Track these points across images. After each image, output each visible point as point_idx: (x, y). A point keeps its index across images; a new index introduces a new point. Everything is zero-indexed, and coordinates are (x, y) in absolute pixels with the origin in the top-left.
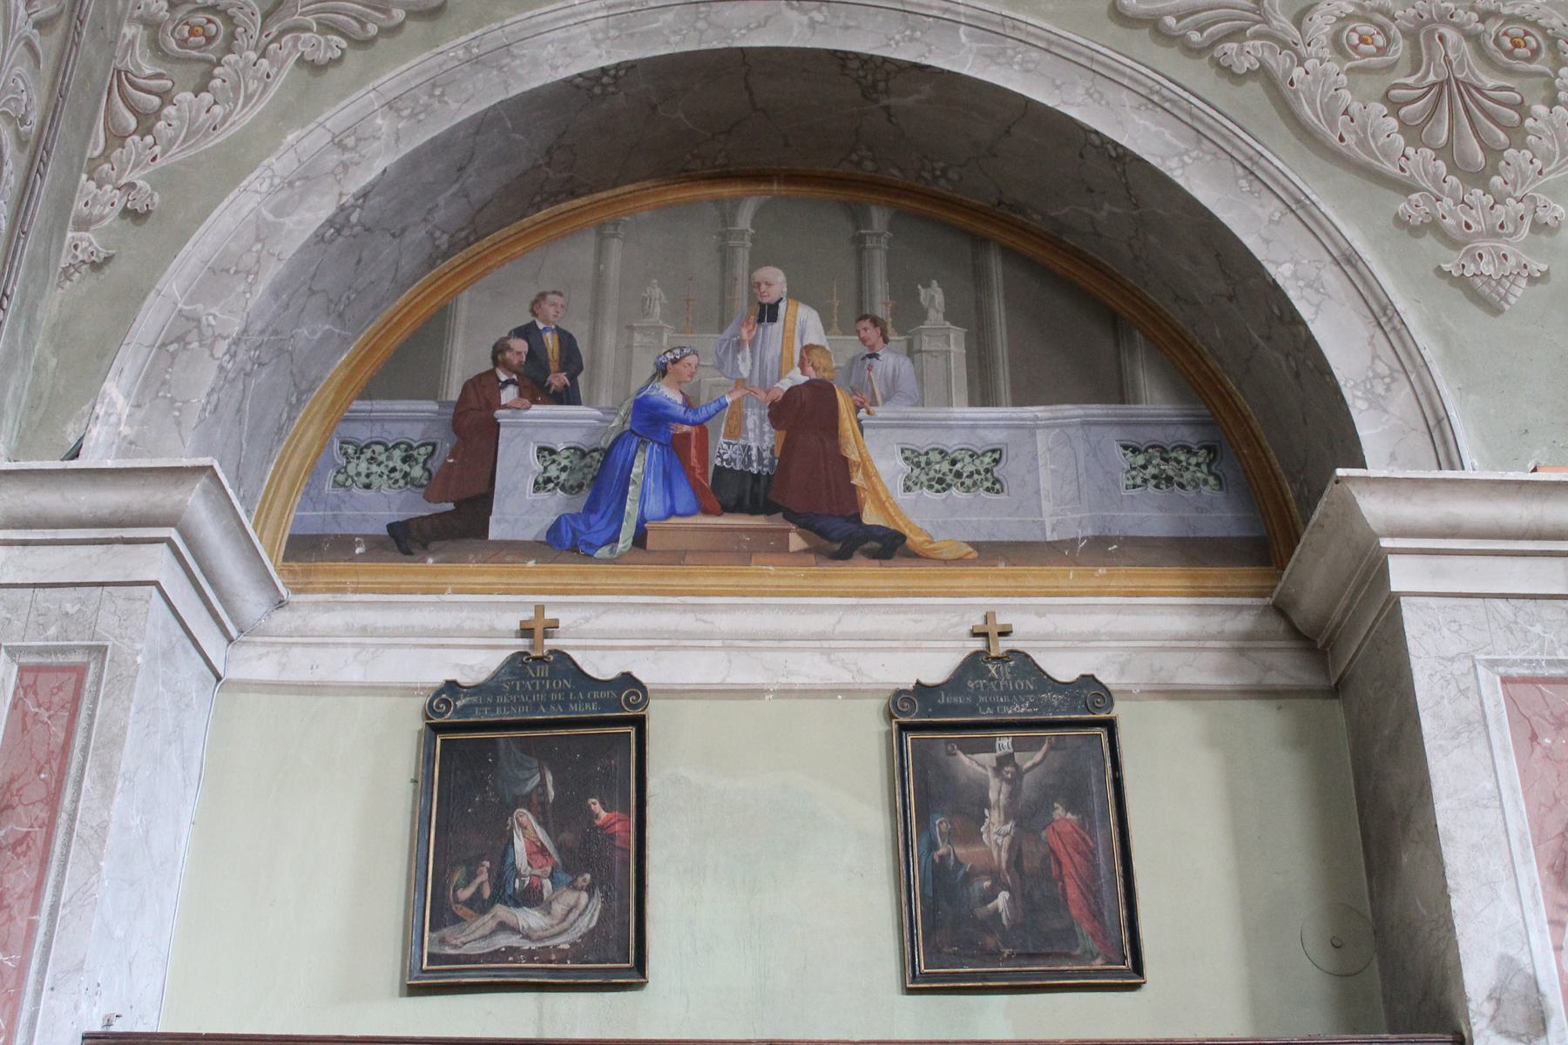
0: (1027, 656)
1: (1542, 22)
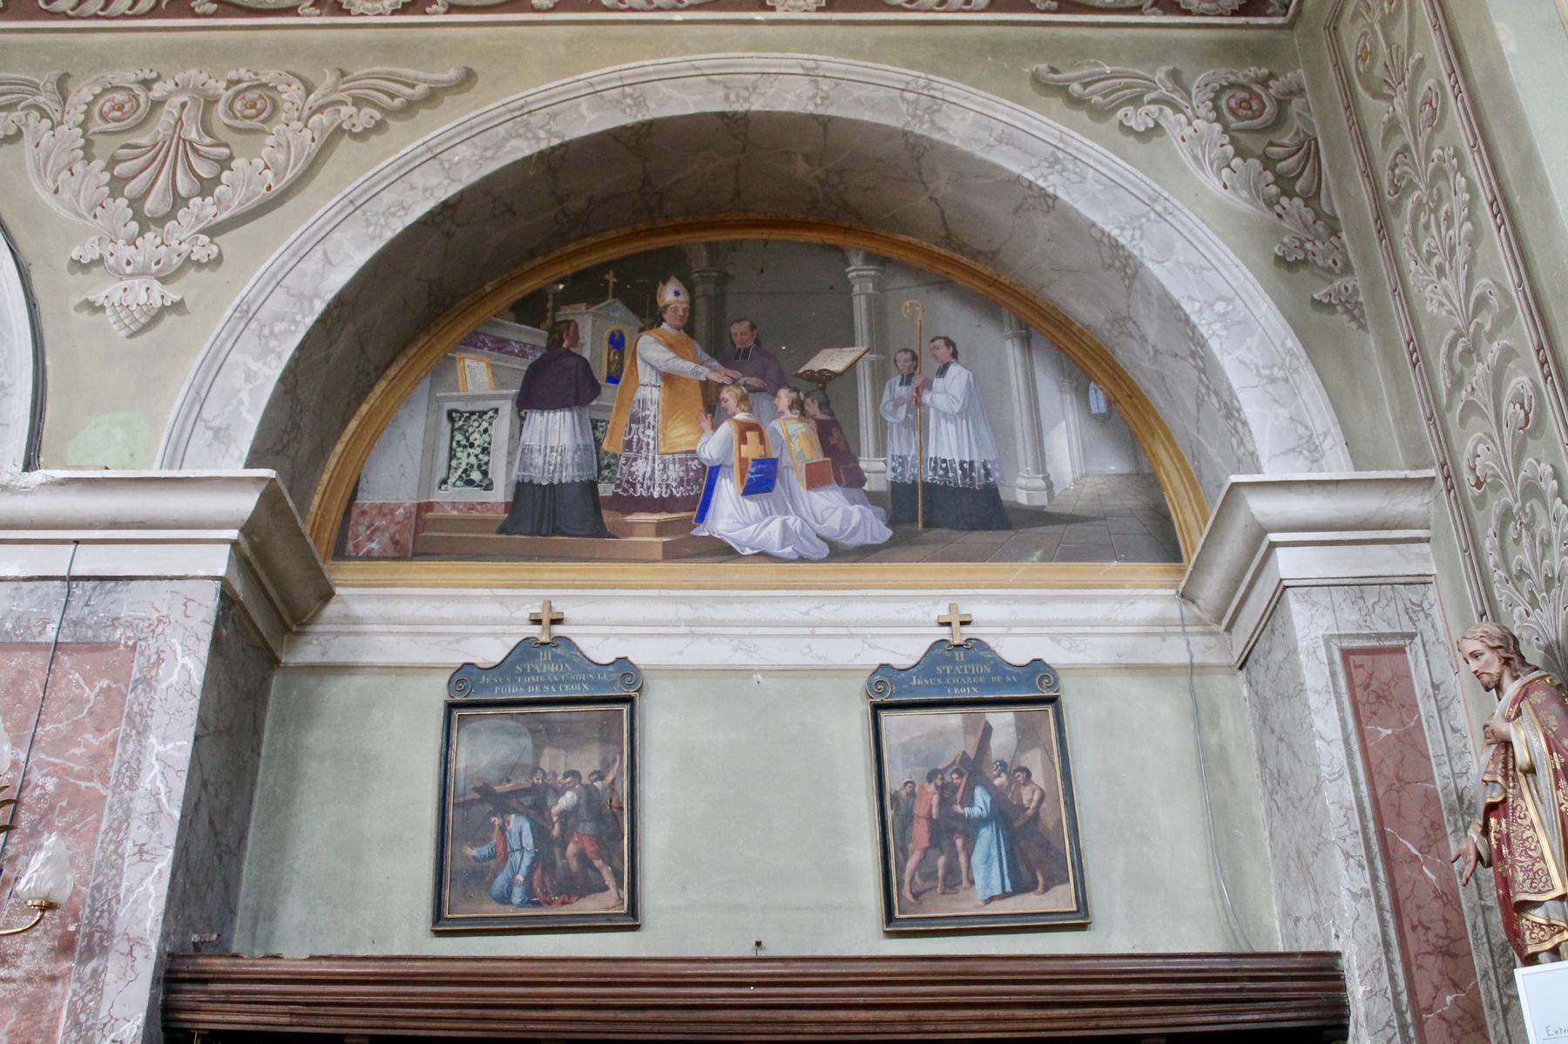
0: (569, 640)
1: (1213, 115)
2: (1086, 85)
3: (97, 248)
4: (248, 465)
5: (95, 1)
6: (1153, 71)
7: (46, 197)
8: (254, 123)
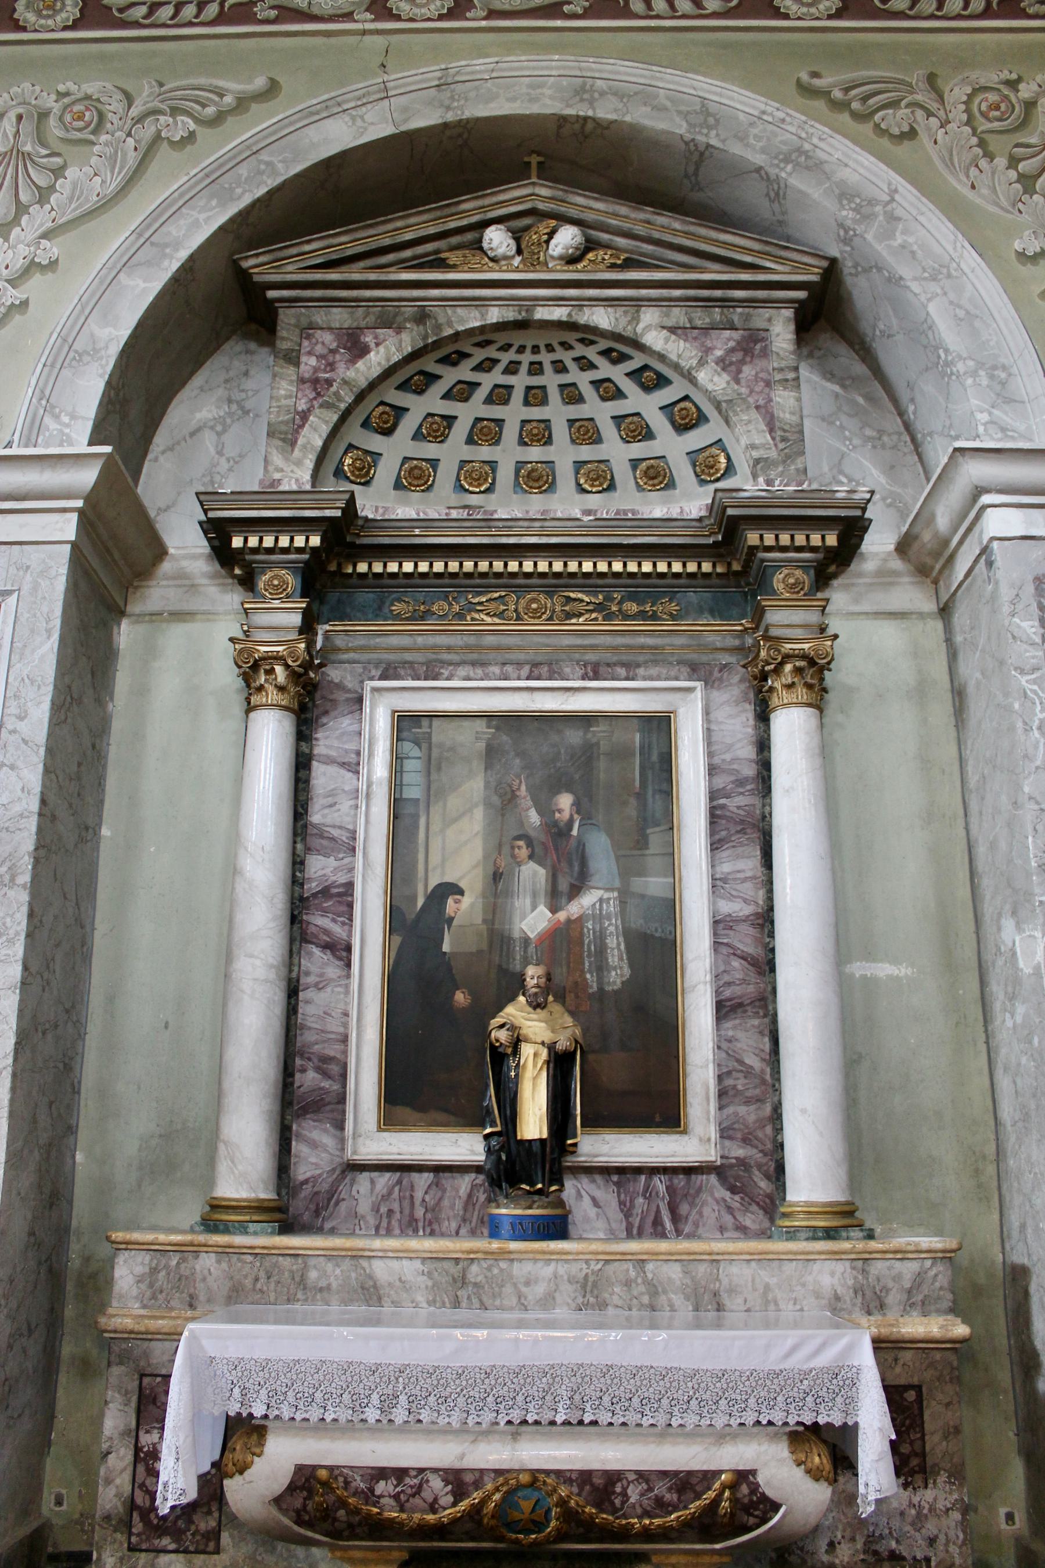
2: (847, 90)
3: (1036, 242)
4: (90, 444)
5: (927, 4)
7: (966, 191)
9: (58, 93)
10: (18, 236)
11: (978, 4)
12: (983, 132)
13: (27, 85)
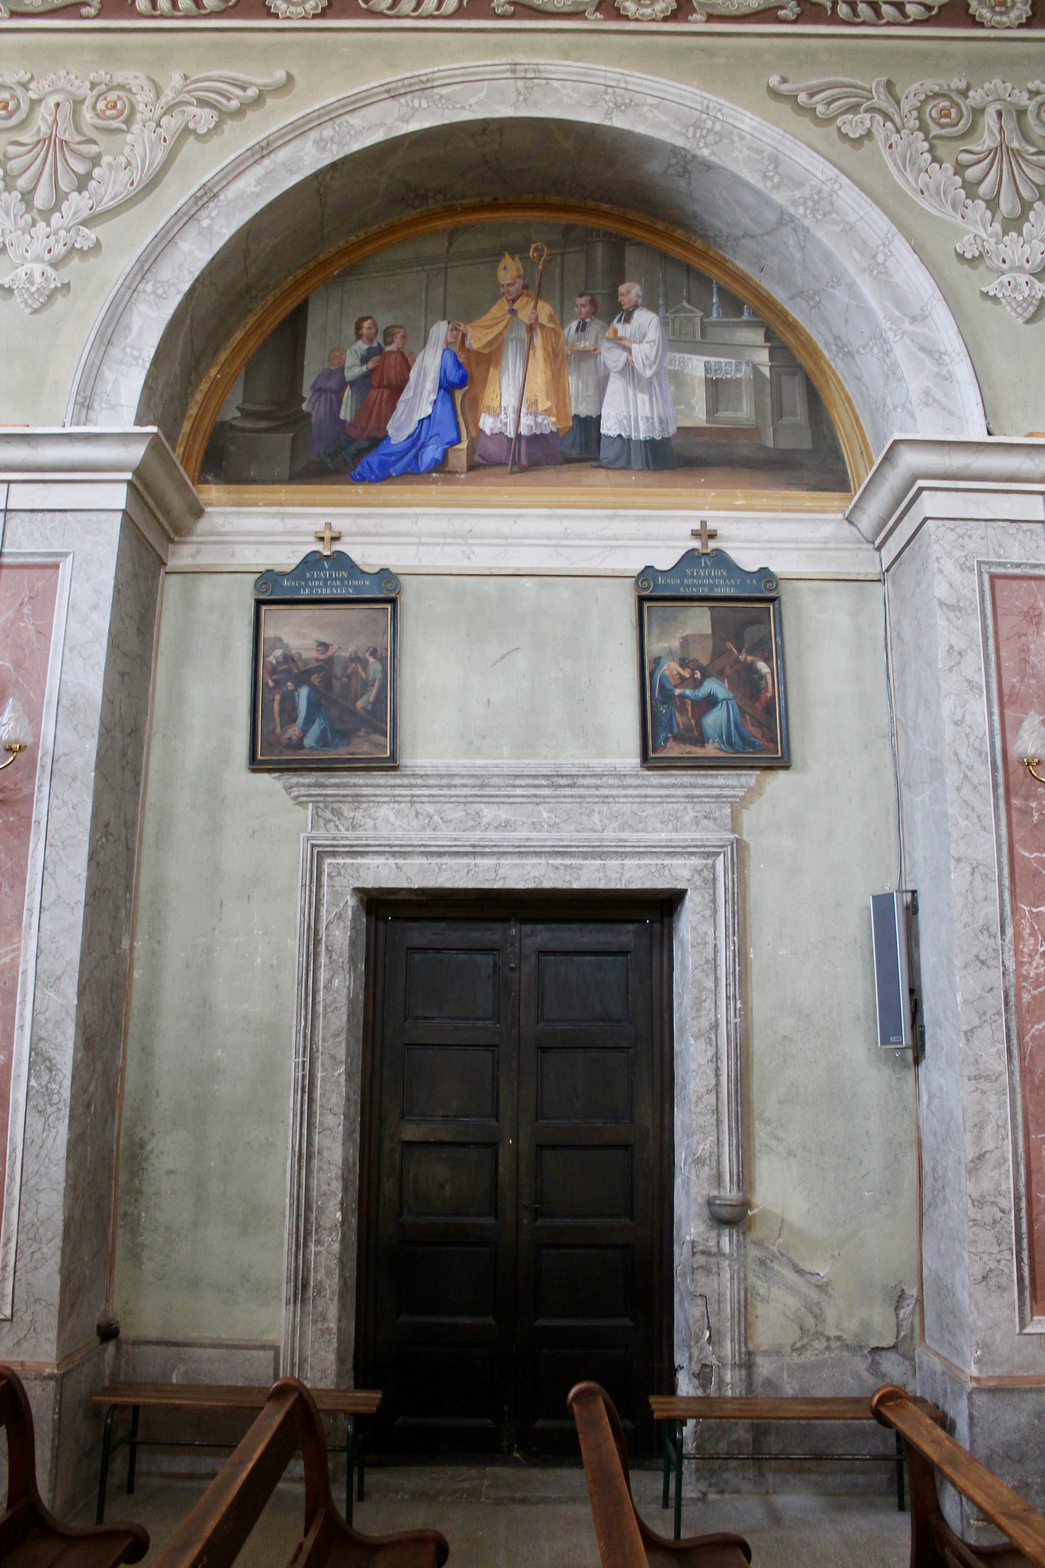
2: (811, 95)
5: (407, 4)
6: (870, 81)
8: (115, 124)
9: (1030, 92)
10: (1030, 231)
11: (452, 1)
12: (934, 137)
13: (997, 81)
